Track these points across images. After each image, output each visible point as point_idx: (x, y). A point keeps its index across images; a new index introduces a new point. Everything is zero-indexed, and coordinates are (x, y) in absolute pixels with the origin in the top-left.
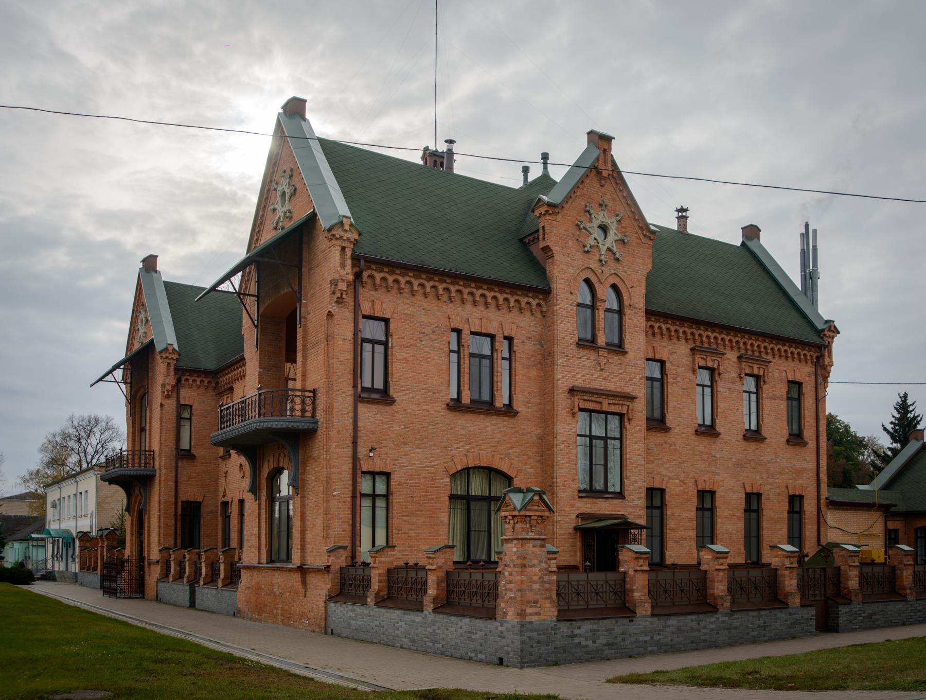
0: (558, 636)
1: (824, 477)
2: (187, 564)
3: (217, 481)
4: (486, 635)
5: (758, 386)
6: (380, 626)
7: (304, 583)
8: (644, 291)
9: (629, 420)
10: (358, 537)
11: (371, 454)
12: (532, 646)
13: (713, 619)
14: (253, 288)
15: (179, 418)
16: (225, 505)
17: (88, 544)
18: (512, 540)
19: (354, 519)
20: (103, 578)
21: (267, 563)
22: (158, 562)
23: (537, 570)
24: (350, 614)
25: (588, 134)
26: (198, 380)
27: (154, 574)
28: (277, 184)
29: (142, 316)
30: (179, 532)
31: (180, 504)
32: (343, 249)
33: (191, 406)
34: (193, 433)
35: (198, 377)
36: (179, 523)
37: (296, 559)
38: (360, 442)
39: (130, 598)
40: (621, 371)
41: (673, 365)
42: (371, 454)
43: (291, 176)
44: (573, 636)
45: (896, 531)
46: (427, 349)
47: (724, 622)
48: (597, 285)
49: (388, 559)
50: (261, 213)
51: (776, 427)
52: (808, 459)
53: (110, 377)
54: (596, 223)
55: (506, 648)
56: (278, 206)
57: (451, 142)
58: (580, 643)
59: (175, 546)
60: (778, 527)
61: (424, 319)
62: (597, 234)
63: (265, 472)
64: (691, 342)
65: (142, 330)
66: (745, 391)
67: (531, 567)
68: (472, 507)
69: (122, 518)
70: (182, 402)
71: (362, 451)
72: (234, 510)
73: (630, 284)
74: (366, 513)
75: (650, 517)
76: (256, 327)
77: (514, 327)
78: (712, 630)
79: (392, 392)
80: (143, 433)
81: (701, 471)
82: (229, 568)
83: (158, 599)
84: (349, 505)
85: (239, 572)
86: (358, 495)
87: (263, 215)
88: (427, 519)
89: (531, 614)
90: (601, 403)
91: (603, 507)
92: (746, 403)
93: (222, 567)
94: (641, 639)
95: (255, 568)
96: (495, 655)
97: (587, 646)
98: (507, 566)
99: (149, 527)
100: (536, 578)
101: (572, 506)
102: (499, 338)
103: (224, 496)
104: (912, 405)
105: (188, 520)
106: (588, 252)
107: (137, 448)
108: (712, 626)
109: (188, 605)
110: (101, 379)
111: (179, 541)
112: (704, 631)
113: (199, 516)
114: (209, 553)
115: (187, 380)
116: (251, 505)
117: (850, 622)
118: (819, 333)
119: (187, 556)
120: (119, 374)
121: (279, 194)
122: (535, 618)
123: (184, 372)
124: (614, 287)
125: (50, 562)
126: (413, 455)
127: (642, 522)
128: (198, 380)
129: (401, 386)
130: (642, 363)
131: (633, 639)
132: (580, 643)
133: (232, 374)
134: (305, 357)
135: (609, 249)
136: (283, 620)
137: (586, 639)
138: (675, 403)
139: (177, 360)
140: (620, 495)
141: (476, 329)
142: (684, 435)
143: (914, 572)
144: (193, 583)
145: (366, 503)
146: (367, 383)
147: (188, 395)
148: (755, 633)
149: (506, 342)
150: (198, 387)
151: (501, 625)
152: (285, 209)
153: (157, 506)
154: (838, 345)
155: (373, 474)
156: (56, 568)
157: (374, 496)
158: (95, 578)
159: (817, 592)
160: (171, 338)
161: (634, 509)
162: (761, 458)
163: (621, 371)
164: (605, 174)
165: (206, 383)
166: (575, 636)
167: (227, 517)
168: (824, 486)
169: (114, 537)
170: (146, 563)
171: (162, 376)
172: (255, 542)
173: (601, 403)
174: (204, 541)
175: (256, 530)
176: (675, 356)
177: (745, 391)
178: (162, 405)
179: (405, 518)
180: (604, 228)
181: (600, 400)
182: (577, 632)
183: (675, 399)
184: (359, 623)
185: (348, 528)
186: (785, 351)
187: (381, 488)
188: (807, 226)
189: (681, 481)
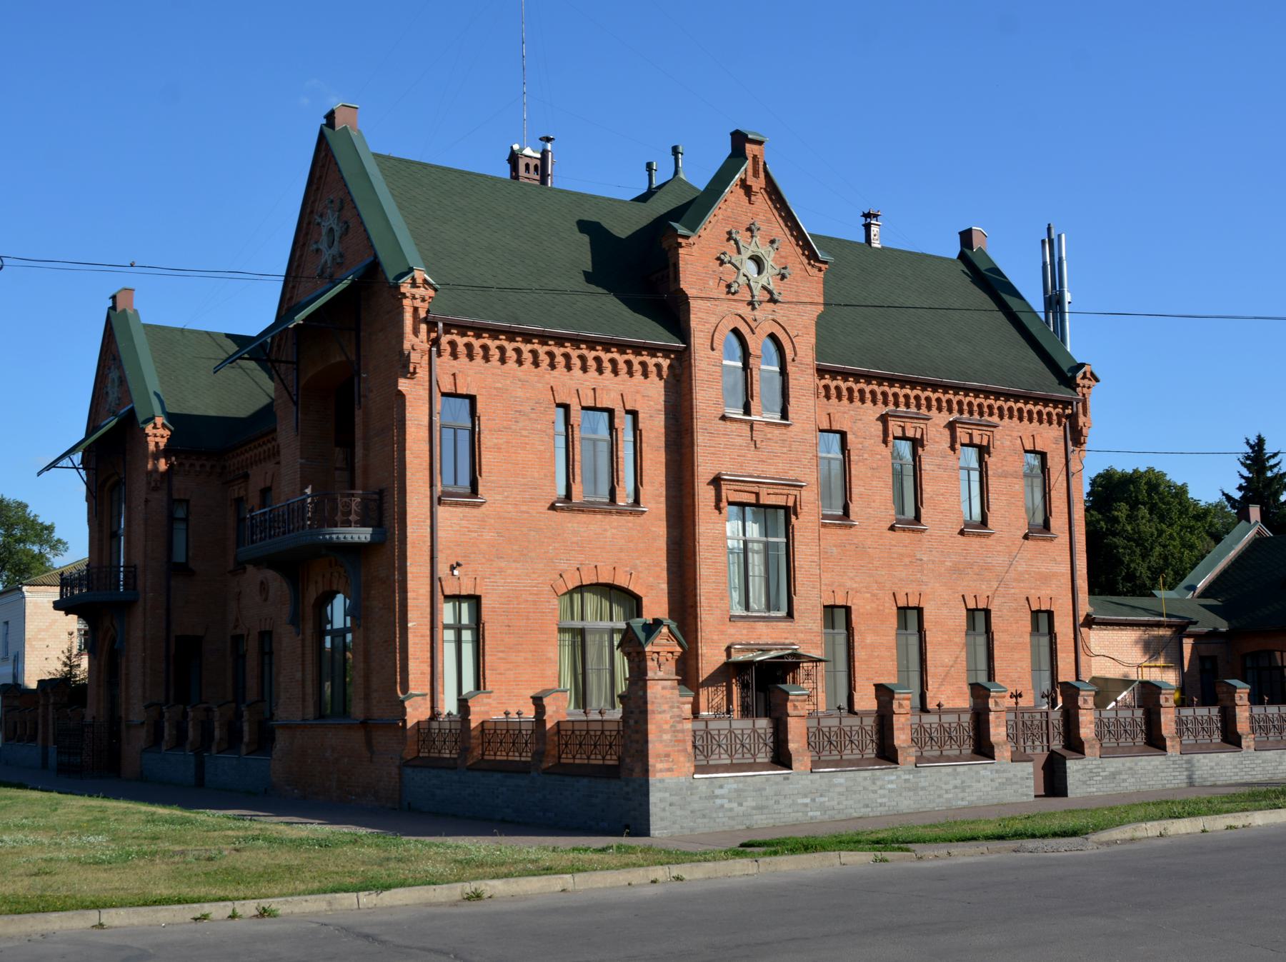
0: (696, 798)
1: (1083, 583)
5: (981, 460)
7: (369, 743)
8: (813, 341)
12: (664, 810)
13: (894, 778)
15: (172, 519)
16: (238, 640)
17: (16, 703)
21: (315, 719)
22: (143, 723)
23: (668, 716)
25: (732, 134)
28: (321, 216)
29: (114, 375)
33: (187, 501)
37: (357, 710)
40: (785, 450)
41: (857, 437)
43: (341, 209)
45: (1213, 659)
46: (525, 433)
47: (906, 780)
49: (483, 709)
50: (298, 254)
52: (1059, 559)
53: (66, 462)
54: (746, 254)
56: (323, 246)
58: (722, 806)
60: (1017, 656)
61: (520, 393)
62: (751, 268)
63: (312, 594)
66: (962, 468)
70: (176, 496)
71: (443, 570)
72: (252, 647)
74: (449, 651)
75: (830, 645)
76: (296, 403)
77: (639, 397)
78: (891, 791)
81: (901, 580)
84: (428, 639)
86: (440, 626)
87: (301, 256)
88: (529, 655)
89: (661, 771)
90: (757, 494)
92: (964, 485)
93: (246, 728)
94: (800, 801)
97: (731, 810)
100: (666, 727)
102: (619, 412)
103: (236, 627)
104: (1275, 455)
105: (183, 659)
108: (890, 786)
111: (172, 693)
117: (1084, 783)
119: (191, 714)
120: (77, 458)
121: (324, 231)
122: (666, 775)
126: (510, 572)
127: (816, 653)
129: (492, 482)
130: (811, 436)
131: (789, 801)
132: (722, 806)
133: (247, 455)
134: (366, 448)
137: (730, 801)
138: (862, 489)
142: (875, 532)
143: (1252, 717)
145: (449, 635)
148: (950, 796)
149: (629, 418)
151: (627, 785)
152: (334, 250)
155: (456, 598)
159: (1037, 743)
161: (805, 634)
162: (989, 560)
163: (785, 450)
166: (717, 797)
167: (240, 658)
168: (1083, 596)
170: (123, 727)
175: (299, 675)
176: (859, 424)
177: (962, 468)
178: (147, 501)
179: (501, 655)
180: (757, 260)
181: (756, 489)
183: (861, 483)
185: (428, 670)
186: (1020, 410)
188: (1049, 229)
189: (873, 595)
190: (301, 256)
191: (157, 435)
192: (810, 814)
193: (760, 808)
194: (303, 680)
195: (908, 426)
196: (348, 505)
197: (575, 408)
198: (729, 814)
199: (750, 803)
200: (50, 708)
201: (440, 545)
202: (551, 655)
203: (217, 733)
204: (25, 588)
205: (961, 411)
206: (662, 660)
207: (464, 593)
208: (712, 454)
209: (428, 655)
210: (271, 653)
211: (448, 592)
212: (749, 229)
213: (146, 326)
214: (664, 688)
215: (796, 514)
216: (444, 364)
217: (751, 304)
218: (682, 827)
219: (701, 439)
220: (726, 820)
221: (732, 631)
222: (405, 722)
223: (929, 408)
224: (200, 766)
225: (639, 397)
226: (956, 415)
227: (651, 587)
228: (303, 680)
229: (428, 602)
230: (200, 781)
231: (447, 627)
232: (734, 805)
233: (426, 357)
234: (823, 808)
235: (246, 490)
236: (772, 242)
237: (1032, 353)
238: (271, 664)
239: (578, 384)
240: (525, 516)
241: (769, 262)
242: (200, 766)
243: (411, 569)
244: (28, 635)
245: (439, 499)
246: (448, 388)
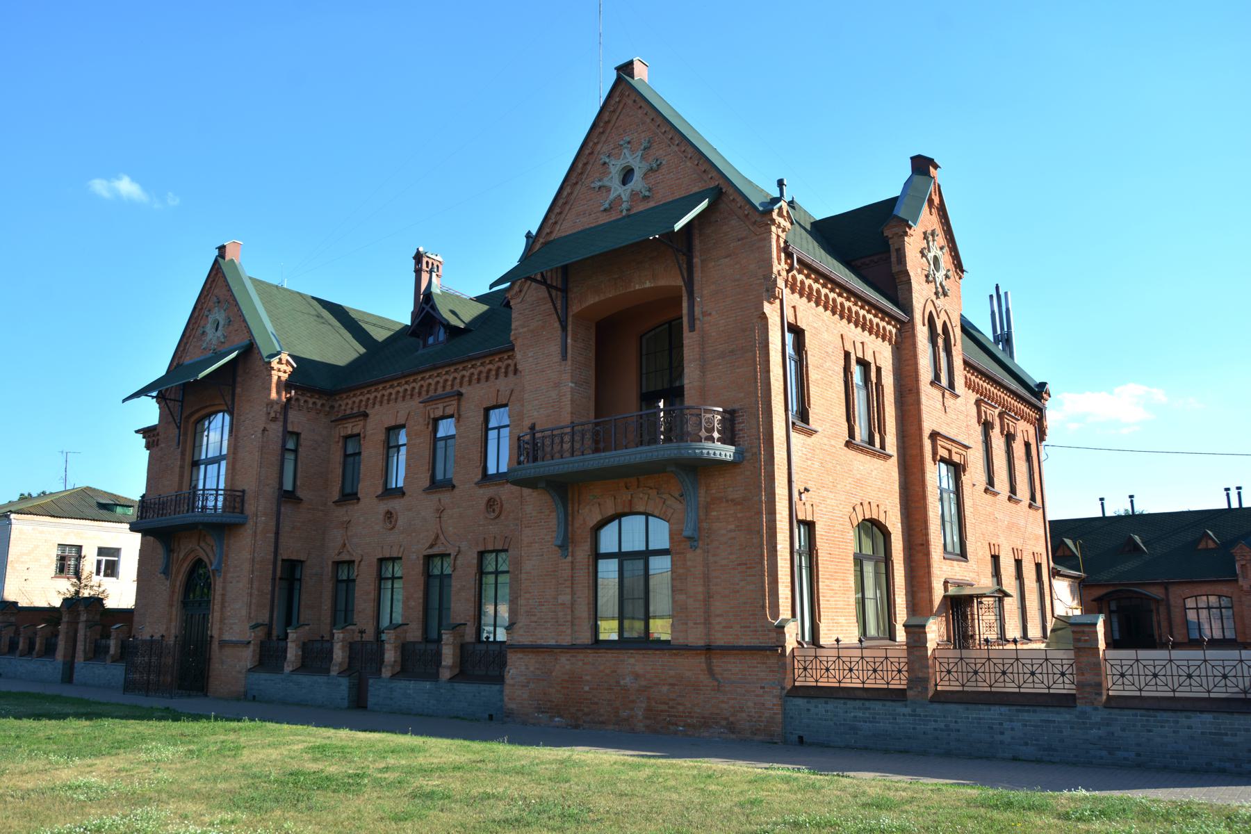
10: (296, 593)
15: (284, 450)
17: (13, 619)
26: (311, 401)
31: (279, 563)
34: (299, 470)
35: (312, 397)
70: (290, 429)
80: (195, 469)
87: (570, 194)
90: (950, 451)
93: (112, 643)
95: (584, 647)
99: (223, 595)
103: (340, 553)
128: (319, 403)
150: (309, 410)
165: (319, 406)
170: (215, 646)
175: (565, 598)
178: (264, 430)
188: (997, 287)
190: (570, 194)
191: (281, 369)
196: (710, 421)
200: (81, 626)
204: (12, 516)
218: (1138, 755)
221: (945, 568)
222: (784, 648)
235: (364, 427)
243: (778, 491)
244: (10, 558)
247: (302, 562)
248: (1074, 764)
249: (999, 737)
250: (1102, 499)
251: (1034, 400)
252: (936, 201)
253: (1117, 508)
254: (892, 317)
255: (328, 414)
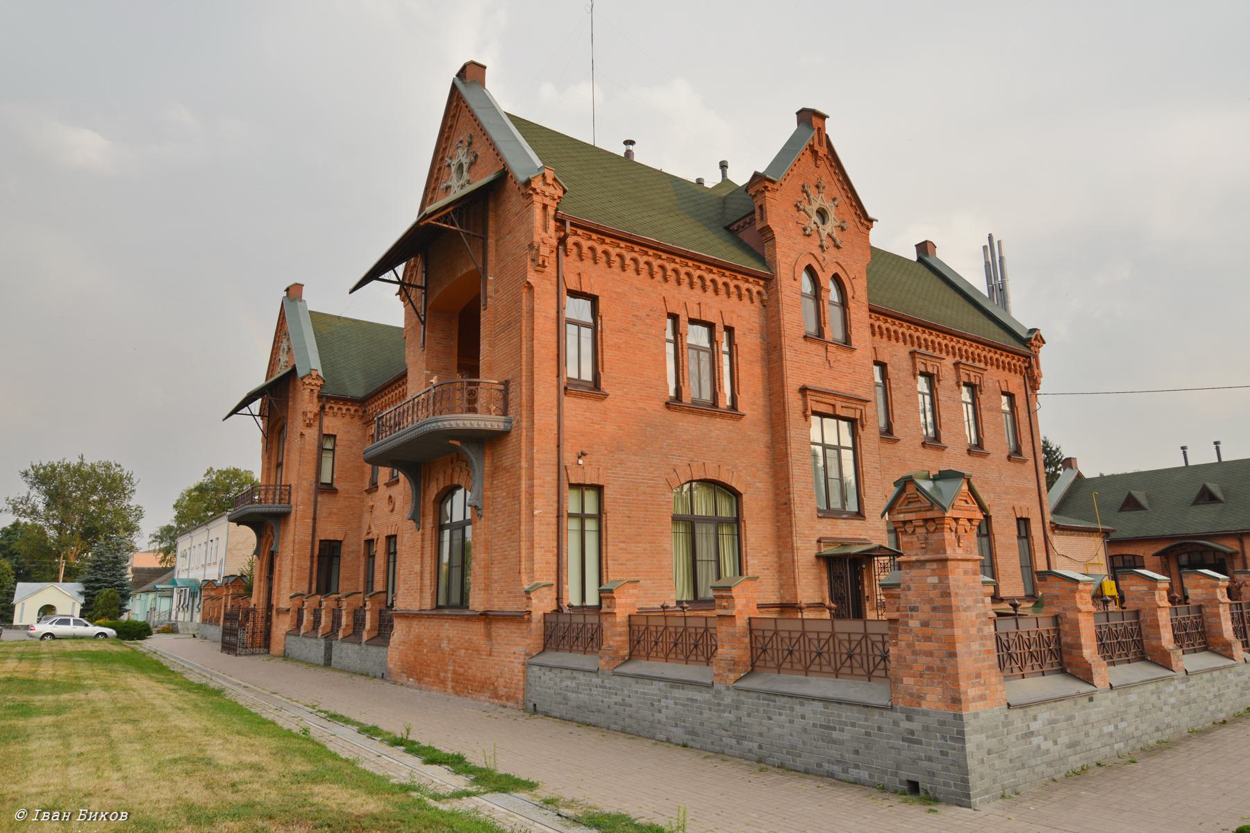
0: (1012, 738)
2: (323, 613)
3: (361, 517)
4: (868, 734)
6: (623, 704)
7: (489, 636)
9: (862, 426)
11: (581, 462)
14: (419, 279)
15: (321, 449)
16: (370, 542)
17: (213, 593)
18: (922, 563)
19: (559, 547)
20: (226, 632)
24: (568, 683)
26: (344, 408)
27: (282, 626)
29: (284, 345)
30: (315, 575)
31: (317, 543)
32: (545, 207)
33: (335, 436)
36: (315, 565)
38: (566, 446)
39: (253, 654)
42: (581, 462)
44: (1030, 734)
46: (641, 336)
48: (820, 273)
49: (629, 601)
51: (998, 441)
53: (245, 410)
54: (815, 207)
55: (925, 764)
57: (631, 143)
59: (310, 591)
63: (433, 491)
64: (909, 344)
65: (283, 358)
67: (965, 610)
68: (698, 531)
69: (251, 563)
70: (325, 432)
71: (569, 458)
72: (380, 549)
73: (852, 276)
76: (423, 323)
77: (734, 316)
78: (1173, 706)
79: (603, 385)
82: (377, 616)
83: (285, 656)
84: (554, 528)
85: (391, 621)
90: (834, 406)
91: (845, 529)
93: (368, 616)
96: (896, 774)
97: (1048, 751)
98: (913, 609)
101: (812, 528)
102: (719, 328)
106: (809, 235)
107: (272, 482)
108: (1172, 700)
109: (322, 661)
110: (235, 411)
111: (314, 586)
112: (1167, 709)
113: (339, 557)
114: (352, 598)
115: (331, 408)
116: (409, 539)
118: (1025, 342)
119: (324, 604)
120: (256, 406)
122: (980, 704)
123: (326, 399)
124: (836, 278)
125: (174, 613)
126: (629, 464)
132: (1039, 747)
135: (829, 235)
136: (453, 688)
139: (321, 386)
140: (860, 515)
141: (695, 316)
144: (331, 635)
145: (573, 525)
146: (572, 372)
147: (332, 424)
150: (343, 416)
153: (290, 547)
154: (1045, 356)
156: (180, 618)
157: (582, 517)
158: (216, 631)
160: (315, 363)
164: (821, 154)
167: (371, 557)
169: (240, 585)
171: (305, 402)
172: (416, 583)
173: (834, 406)
174: (345, 586)
175: (417, 568)
180: (822, 213)
181: (832, 402)
182: (1034, 726)
184: (583, 697)
185: (553, 559)
187: (591, 508)
188: (990, 237)
192: (1116, 746)
193: (1073, 745)
194: (422, 573)
195: (929, 363)
197: (683, 320)
198: (1046, 758)
199: (1064, 739)
201: (566, 435)
202: (667, 546)
203: (344, 621)
205: (961, 357)
206: (961, 531)
207: (588, 482)
208: (803, 365)
209: (555, 544)
210: (395, 553)
211: (573, 481)
212: (817, 187)
213: (313, 314)
214: (966, 573)
215: (862, 426)
216: (570, 264)
217: (821, 246)
218: (760, 747)
219: (788, 354)
220: (1043, 768)
223: (941, 351)
224: (329, 649)
225: (734, 316)
226: (958, 358)
227: (748, 485)
228: (422, 573)
229: (554, 490)
230: (328, 662)
231: (571, 516)
232: (1049, 744)
233: (554, 255)
234: (1126, 738)
236: (834, 200)
237: (991, 323)
238: (395, 562)
239: (686, 299)
240: (643, 412)
241: (832, 214)
242: (329, 649)
245: (566, 388)
246: (573, 286)
247: (341, 542)
248: (720, 753)
249: (657, 716)
250: (1183, 448)
251: (1022, 349)
252: (822, 151)
253: (1202, 456)
254: (747, 274)
255: (362, 418)
